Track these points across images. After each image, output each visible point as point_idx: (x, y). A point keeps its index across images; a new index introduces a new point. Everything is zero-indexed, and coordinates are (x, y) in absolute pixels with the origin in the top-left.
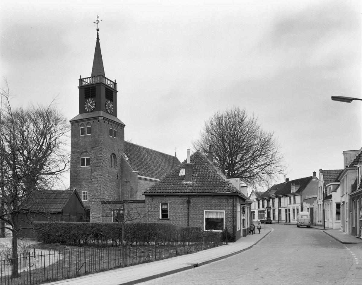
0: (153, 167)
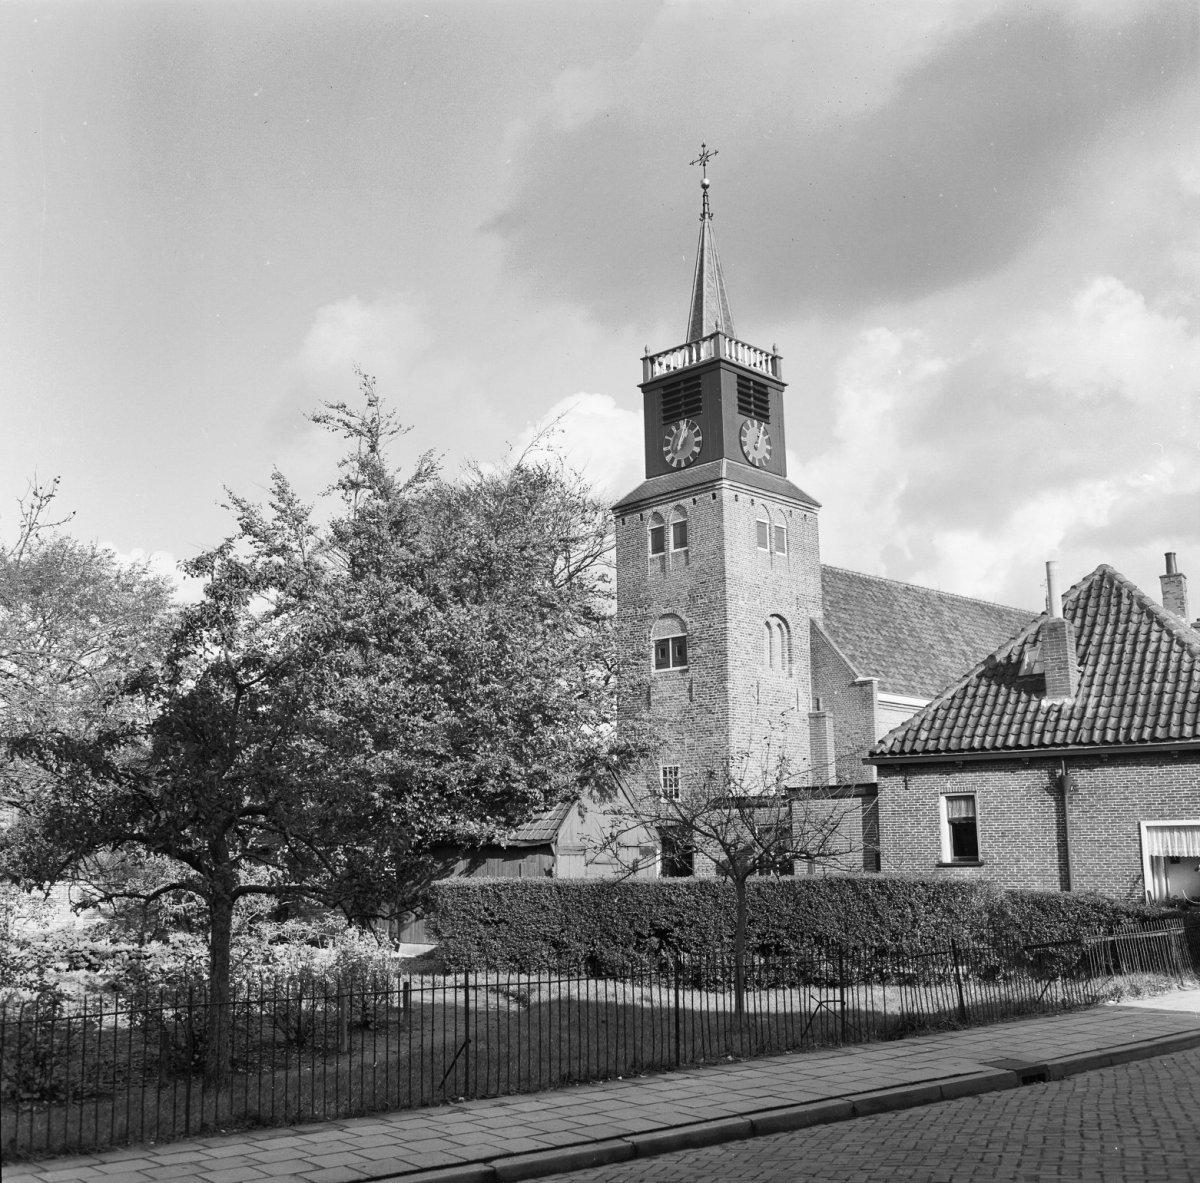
0: (945, 660)
